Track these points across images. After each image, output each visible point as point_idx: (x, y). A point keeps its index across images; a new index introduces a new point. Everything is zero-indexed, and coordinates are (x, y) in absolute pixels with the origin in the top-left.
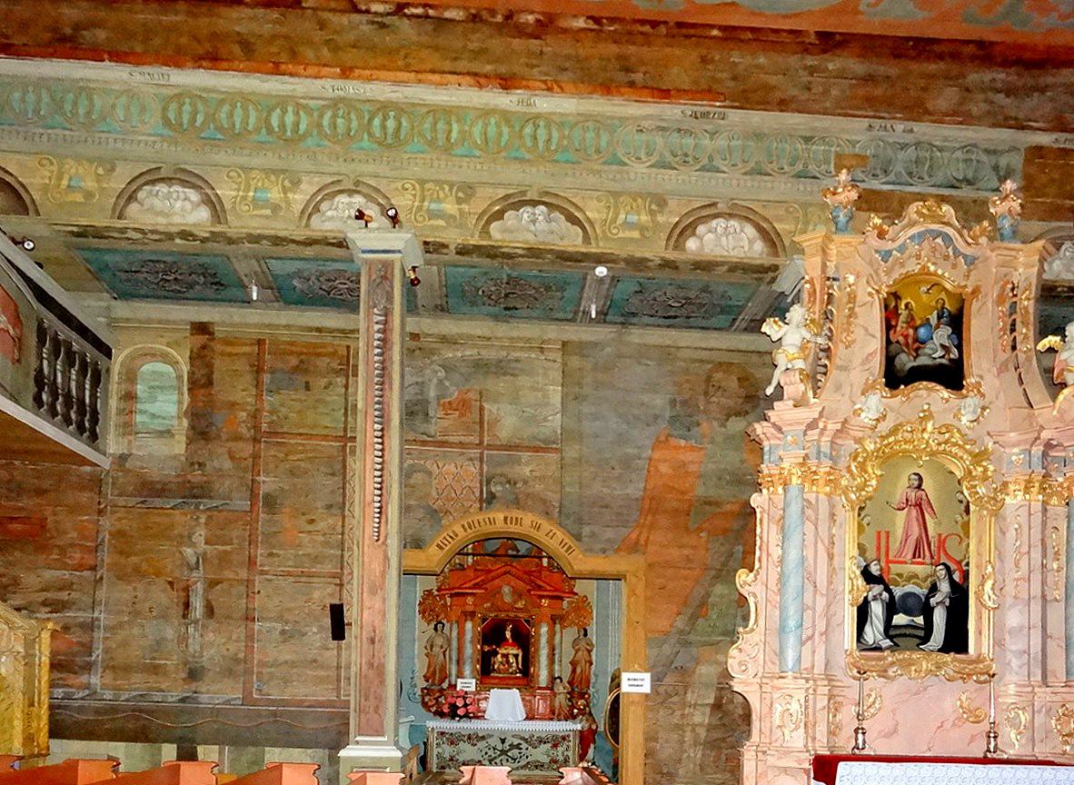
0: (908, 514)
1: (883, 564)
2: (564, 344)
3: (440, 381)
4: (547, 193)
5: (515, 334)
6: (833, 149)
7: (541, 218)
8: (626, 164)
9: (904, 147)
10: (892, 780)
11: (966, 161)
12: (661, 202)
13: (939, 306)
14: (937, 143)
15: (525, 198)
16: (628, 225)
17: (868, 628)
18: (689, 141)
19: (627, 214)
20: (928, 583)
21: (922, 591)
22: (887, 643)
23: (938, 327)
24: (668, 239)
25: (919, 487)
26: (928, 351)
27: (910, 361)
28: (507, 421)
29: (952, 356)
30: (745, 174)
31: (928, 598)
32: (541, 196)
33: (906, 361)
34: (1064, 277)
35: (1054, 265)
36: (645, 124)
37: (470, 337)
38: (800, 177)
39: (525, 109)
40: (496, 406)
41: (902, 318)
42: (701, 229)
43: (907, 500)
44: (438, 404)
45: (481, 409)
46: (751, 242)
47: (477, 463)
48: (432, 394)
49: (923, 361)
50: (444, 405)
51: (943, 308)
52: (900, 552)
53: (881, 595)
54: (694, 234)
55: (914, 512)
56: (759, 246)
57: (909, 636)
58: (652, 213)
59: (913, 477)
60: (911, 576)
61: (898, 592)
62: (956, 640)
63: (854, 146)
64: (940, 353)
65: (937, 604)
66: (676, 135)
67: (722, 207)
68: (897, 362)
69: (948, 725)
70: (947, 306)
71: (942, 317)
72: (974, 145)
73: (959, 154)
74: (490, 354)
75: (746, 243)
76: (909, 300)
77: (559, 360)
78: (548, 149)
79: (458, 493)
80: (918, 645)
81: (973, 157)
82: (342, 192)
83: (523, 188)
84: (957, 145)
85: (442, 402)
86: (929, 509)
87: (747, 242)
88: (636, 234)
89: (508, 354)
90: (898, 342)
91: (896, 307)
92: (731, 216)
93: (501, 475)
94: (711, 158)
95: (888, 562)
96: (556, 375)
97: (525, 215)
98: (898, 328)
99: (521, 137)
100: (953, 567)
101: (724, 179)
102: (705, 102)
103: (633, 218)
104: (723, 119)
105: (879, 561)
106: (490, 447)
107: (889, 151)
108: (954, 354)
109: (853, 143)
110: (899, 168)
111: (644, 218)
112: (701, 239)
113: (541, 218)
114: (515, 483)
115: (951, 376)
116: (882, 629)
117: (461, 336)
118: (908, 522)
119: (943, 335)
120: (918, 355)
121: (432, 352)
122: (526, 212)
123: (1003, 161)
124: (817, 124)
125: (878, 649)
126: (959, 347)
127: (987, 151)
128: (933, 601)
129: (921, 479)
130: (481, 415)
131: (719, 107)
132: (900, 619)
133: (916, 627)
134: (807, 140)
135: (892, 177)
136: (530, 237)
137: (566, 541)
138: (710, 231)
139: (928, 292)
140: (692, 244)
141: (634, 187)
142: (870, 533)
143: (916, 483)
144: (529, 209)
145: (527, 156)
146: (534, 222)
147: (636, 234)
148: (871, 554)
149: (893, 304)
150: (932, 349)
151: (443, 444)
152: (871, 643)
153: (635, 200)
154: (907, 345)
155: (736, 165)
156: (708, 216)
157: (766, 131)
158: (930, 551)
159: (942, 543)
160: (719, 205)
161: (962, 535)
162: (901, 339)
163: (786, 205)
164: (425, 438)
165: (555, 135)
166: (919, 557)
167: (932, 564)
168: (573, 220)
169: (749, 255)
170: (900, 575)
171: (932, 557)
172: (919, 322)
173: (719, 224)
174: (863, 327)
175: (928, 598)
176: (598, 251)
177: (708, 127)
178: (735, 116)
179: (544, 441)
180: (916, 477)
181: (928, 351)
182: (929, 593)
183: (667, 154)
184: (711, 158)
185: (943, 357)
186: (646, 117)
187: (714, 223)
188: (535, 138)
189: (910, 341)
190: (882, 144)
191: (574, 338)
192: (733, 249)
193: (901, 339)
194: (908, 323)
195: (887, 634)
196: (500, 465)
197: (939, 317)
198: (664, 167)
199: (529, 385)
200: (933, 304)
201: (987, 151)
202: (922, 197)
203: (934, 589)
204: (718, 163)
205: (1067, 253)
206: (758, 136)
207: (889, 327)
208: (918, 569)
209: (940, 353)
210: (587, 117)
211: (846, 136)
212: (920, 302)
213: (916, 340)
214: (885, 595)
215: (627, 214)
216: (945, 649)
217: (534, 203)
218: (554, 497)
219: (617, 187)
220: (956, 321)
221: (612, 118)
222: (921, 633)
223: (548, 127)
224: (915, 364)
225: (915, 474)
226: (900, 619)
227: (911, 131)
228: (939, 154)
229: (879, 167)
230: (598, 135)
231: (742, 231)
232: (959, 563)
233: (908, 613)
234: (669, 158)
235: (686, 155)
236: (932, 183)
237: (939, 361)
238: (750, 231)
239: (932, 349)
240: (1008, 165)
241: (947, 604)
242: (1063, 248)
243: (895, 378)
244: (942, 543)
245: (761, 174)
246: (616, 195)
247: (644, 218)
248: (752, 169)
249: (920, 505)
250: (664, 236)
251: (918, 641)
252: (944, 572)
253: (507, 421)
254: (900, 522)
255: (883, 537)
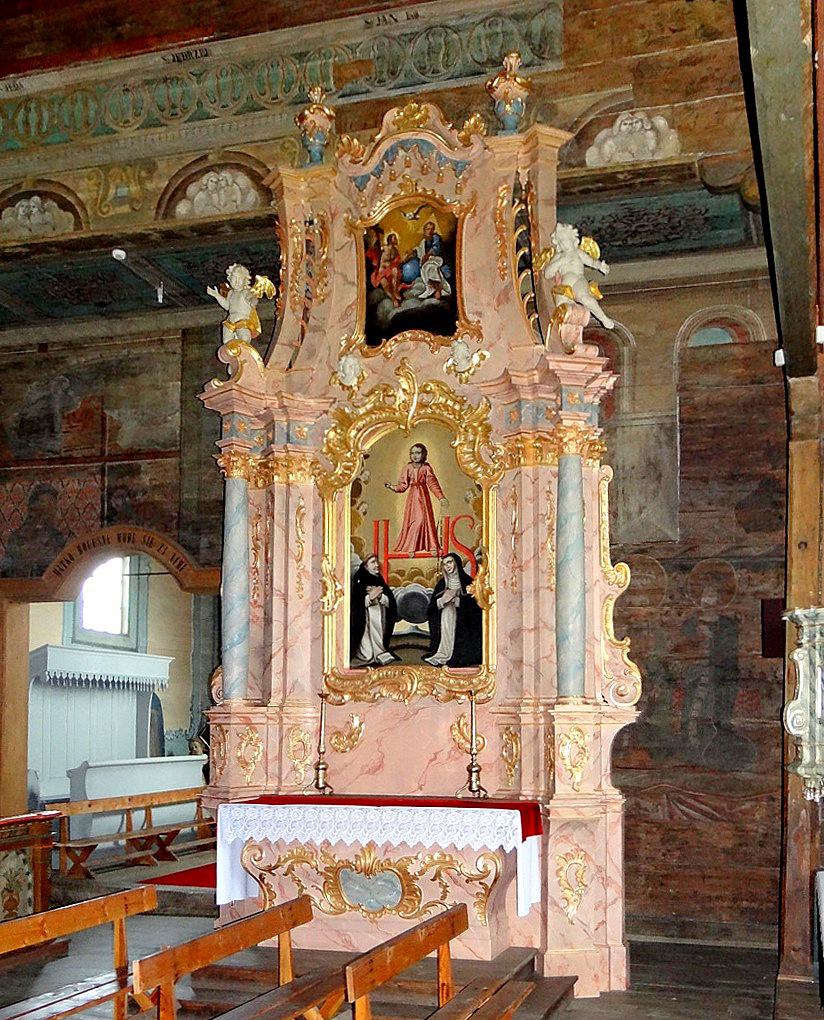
0: (411, 497)
1: (382, 561)
2: (185, 332)
3: (66, 392)
4: (41, 181)
5: (134, 329)
6: (331, 60)
7: (35, 210)
8: (115, 132)
9: (412, 37)
10: (381, 827)
11: (489, 36)
12: (150, 166)
13: (428, 232)
14: (451, 24)
15: (21, 191)
16: (119, 200)
17: (365, 640)
18: (176, 90)
19: (117, 188)
20: (434, 581)
21: (426, 591)
22: (387, 657)
23: (426, 259)
24: (159, 206)
25: (423, 461)
26: (414, 292)
27: (394, 308)
28: (129, 431)
29: (444, 293)
30: (238, 113)
31: (434, 598)
32: (35, 186)
33: (390, 308)
34: (618, 159)
35: (606, 147)
36: (130, 81)
37: (93, 339)
38: (296, 104)
39: (16, 94)
40: (117, 412)
41: (384, 256)
42: (192, 189)
43: (409, 479)
44: (63, 417)
45: (103, 418)
46: (244, 194)
47: (98, 477)
48: (57, 407)
49: (410, 304)
50: (68, 417)
51: (432, 234)
52: (401, 546)
53: (379, 599)
54: (184, 197)
55: (417, 493)
56: (253, 196)
57: (414, 647)
58: (141, 181)
59: (416, 449)
60: (414, 573)
61: (399, 593)
62: (469, 652)
63: (354, 52)
64: (429, 292)
65: (446, 605)
66: (162, 86)
67: (212, 159)
68: (380, 311)
69: (443, 757)
70: (437, 230)
71: (431, 246)
72: (498, 15)
73: (480, 30)
74: (111, 356)
75: (238, 196)
76: (393, 232)
77: (179, 351)
78: (39, 132)
79: (81, 512)
80: (423, 658)
81: (499, 30)
82: (207, 170)
83: (18, 181)
84: (477, 19)
85: (66, 415)
86: (435, 488)
87: (239, 193)
88: (126, 209)
89: (129, 352)
90: (380, 286)
91: (378, 244)
92: (223, 167)
93: (122, 487)
94: (200, 104)
95: (388, 557)
96: (175, 368)
97: (21, 211)
98: (381, 269)
99: (13, 124)
100: (463, 557)
101: (215, 125)
102: (360, 8)
103: (123, 191)
104: (206, 55)
105: (377, 556)
106: (112, 458)
107: (396, 48)
108: (446, 292)
109: (352, 49)
110: (410, 65)
111: (134, 188)
112: (192, 200)
113: (35, 210)
114: (135, 496)
115: (441, 319)
116: (381, 641)
117: (85, 339)
118: (410, 506)
119: (432, 268)
120: (403, 299)
121: (58, 361)
122: (21, 207)
123: (536, 25)
124: (308, 35)
125: (377, 665)
126: (452, 281)
127: (516, 18)
128: (440, 602)
129: (424, 451)
130: (103, 424)
131: (207, 41)
132: (402, 627)
133: (421, 636)
134: (301, 56)
135: (401, 79)
136: (25, 233)
137: (178, 555)
138: (201, 190)
139: (414, 218)
140: (182, 209)
141: (122, 155)
142: (367, 523)
143: (419, 456)
144: (24, 203)
145: (20, 145)
146: (28, 215)
147: (126, 209)
148: (368, 550)
149: (374, 240)
150: (418, 288)
151: (70, 460)
152: (369, 658)
153: (125, 171)
154: (391, 287)
155: (128, 121)
156: (199, 171)
157: (256, 58)
158: (437, 542)
159: (450, 526)
160: (210, 157)
161: (474, 516)
162: (384, 282)
163: (281, 141)
164: (51, 455)
165: (46, 114)
166: (424, 548)
167: (438, 556)
168: (65, 206)
169: (241, 209)
170: (401, 573)
171: (438, 547)
172: (404, 257)
173: (209, 179)
174: (341, 274)
175: (434, 598)
176: (89, 235)
177: (194, 69)
178: (218, 49)
179: (164, 445)
180: (419, 450)
181: (414, 292)
182: (435, 593)
183: (155, 109)
184: (200, 104)
185: (433, 296)
186: (133, 72)
187: (204, 179)
188: (26, 123)
189: (394, 282)
190: (386, 41)
191: (191, 324)
192: (225, 205)
193: (384, 282)
194: (390, 260)
195: (387, 647)
196: (121, 476)
197: (428, 247)
198: (155, 126)
199: (148, 383)
200: (421, 231)
201: (516, 18)
202: (400, 102)
203: (441, 587)
204: (209, 108)
205: (623, 128)
206: (248, 66)
207: (370, 269)
208: (426, 564)
209: (429, 292)
210: (73, 89)
211: (343, 42)
212: (408, 234)
213: (401, 280)
214: (385, 598)
215: (117, 188)
216: (453, 663)
217: (28, 195)
218: (170, 507)
219: (106, 158)
220: (448, 249)
221: (97, 82)
222: (427, 643)
223: (38, 108)
224: (398, 310)
225: (417, 445)
226: (402, 627)
227: (417, 16)
228: (455, 36)
229: (385, 70)
230: (86, 104)
231: (234, 182)
232: (471, 552)
233: (410, 619)
234: (157, 114)
235: (174, 107)
236: (449, 76)
237: (427, 302)
238: (243, 180)
239: (418, 288)
240: (543, 31)
241: (457, 604)
242: (618, 122)
243: (377, 331)
244: (450, 526)
245: (255, 110)
246: (105, 168)
247: (134, 188)
248: (245, 106)
249: (424, 484)
250: (154, 205)
251: (422, 653)
252: (452, 565)
253: (129, 431)
254: (401, 508)
255: (382, 527)
